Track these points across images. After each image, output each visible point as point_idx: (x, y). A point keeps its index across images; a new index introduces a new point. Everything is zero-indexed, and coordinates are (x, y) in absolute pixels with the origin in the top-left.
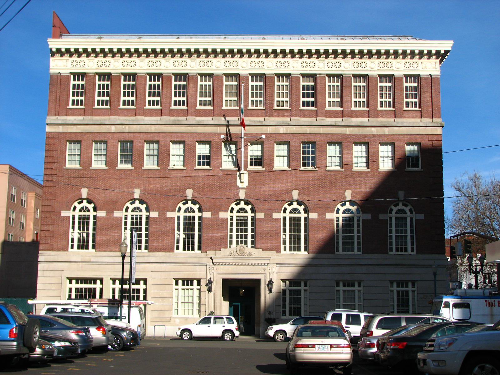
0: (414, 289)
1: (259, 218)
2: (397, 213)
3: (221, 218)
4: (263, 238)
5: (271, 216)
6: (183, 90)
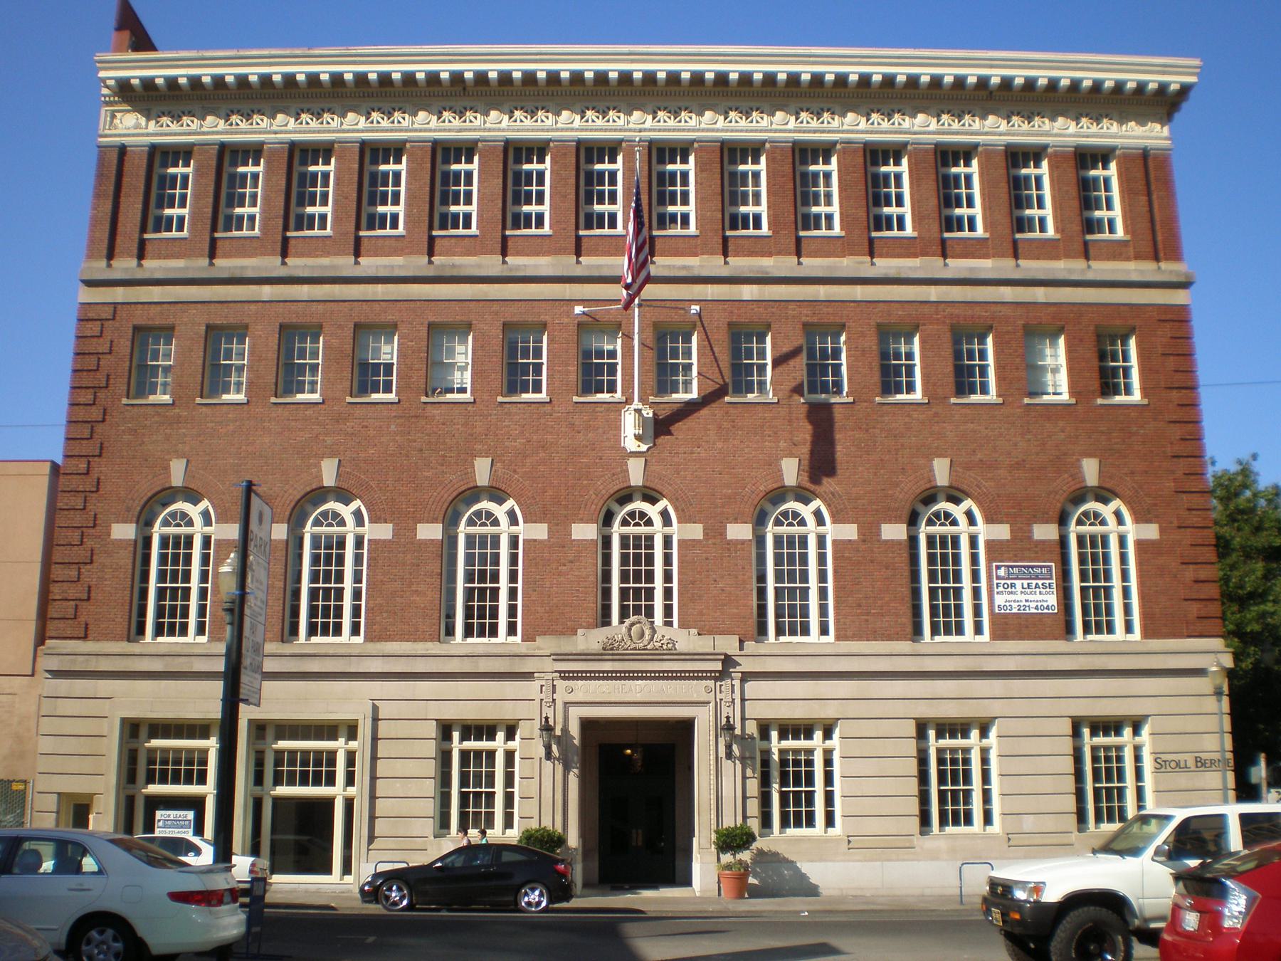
5: (723, 533)
6: (537, 186)
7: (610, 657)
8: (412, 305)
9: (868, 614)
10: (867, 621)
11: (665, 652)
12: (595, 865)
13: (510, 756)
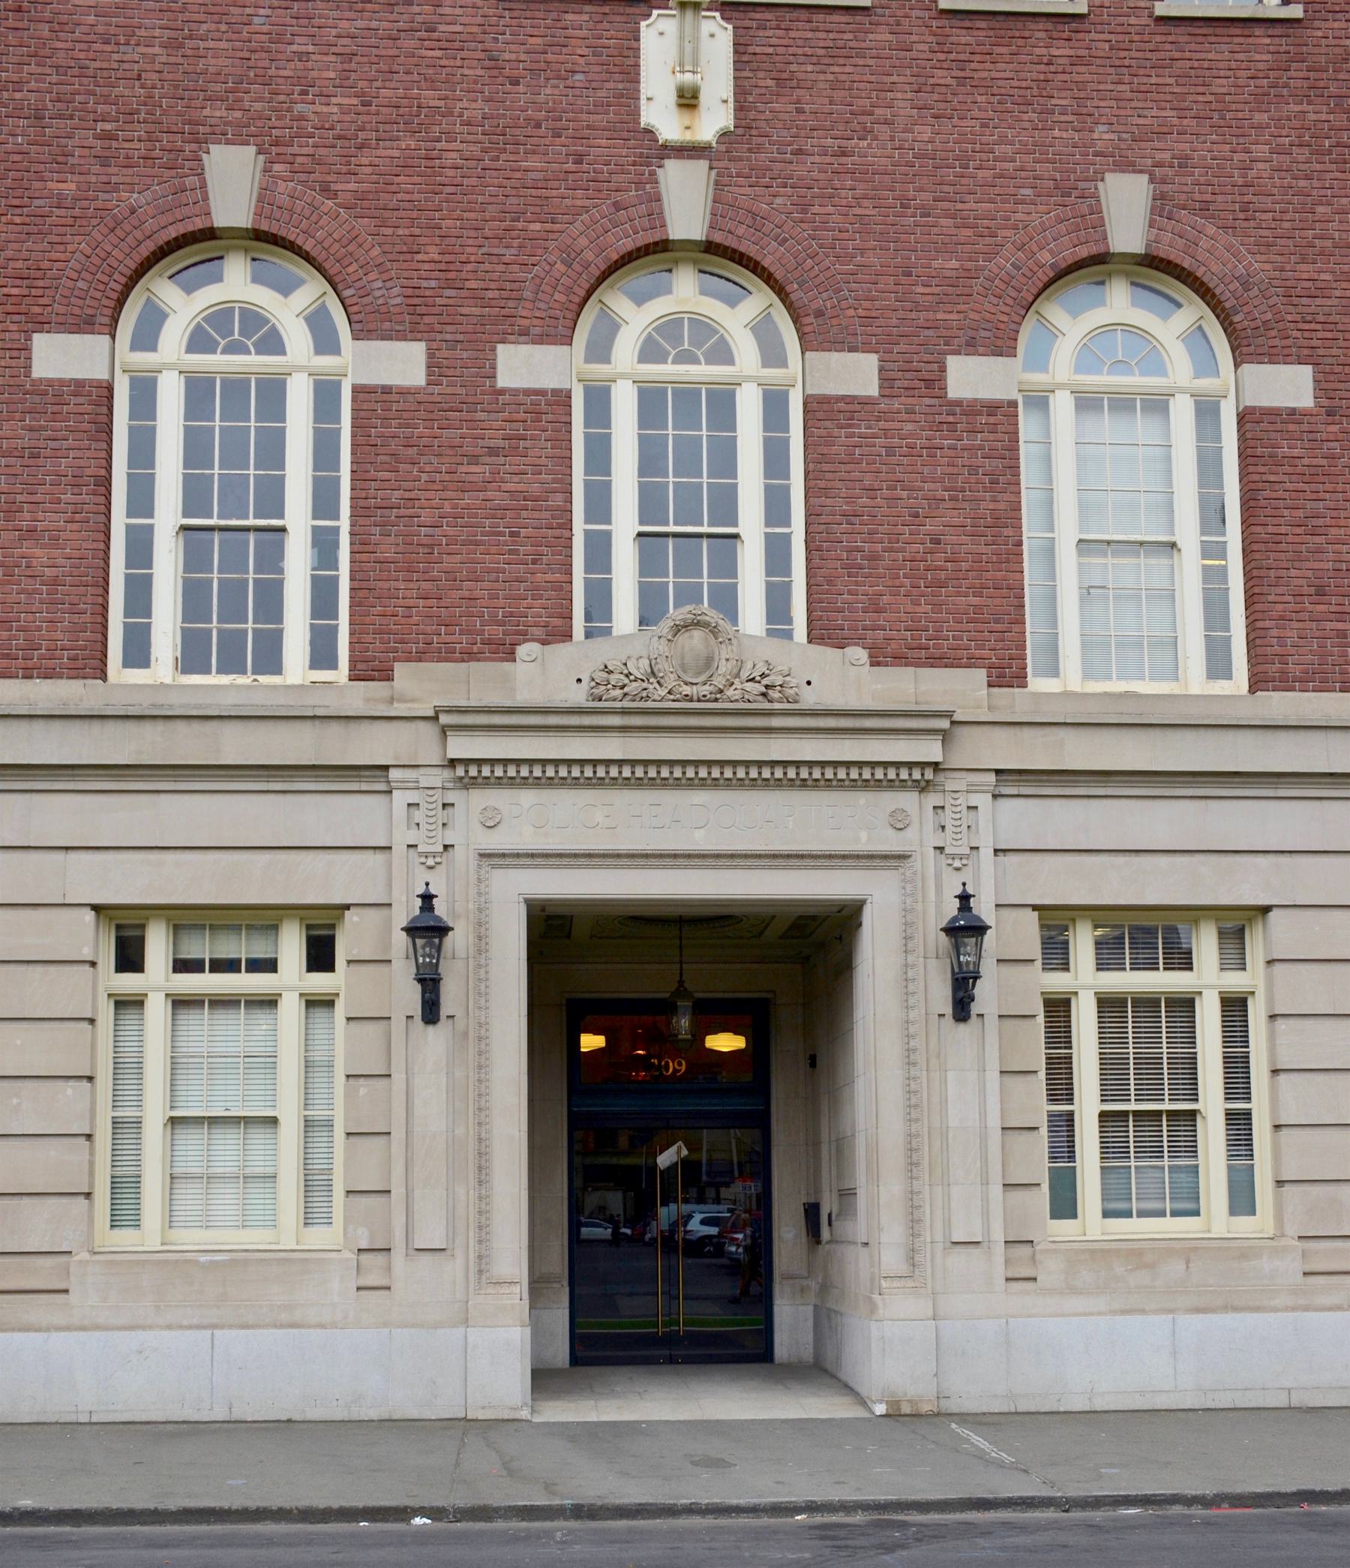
0: (1235, 981)
1: (843, 398)
2: (199, 342)
3: (515, 392)
4: (874, 557)
5: (935, 382)
7: (262, 1223)
11: (777, 706)
12: (559, 1318)
13: (1235, 1006)
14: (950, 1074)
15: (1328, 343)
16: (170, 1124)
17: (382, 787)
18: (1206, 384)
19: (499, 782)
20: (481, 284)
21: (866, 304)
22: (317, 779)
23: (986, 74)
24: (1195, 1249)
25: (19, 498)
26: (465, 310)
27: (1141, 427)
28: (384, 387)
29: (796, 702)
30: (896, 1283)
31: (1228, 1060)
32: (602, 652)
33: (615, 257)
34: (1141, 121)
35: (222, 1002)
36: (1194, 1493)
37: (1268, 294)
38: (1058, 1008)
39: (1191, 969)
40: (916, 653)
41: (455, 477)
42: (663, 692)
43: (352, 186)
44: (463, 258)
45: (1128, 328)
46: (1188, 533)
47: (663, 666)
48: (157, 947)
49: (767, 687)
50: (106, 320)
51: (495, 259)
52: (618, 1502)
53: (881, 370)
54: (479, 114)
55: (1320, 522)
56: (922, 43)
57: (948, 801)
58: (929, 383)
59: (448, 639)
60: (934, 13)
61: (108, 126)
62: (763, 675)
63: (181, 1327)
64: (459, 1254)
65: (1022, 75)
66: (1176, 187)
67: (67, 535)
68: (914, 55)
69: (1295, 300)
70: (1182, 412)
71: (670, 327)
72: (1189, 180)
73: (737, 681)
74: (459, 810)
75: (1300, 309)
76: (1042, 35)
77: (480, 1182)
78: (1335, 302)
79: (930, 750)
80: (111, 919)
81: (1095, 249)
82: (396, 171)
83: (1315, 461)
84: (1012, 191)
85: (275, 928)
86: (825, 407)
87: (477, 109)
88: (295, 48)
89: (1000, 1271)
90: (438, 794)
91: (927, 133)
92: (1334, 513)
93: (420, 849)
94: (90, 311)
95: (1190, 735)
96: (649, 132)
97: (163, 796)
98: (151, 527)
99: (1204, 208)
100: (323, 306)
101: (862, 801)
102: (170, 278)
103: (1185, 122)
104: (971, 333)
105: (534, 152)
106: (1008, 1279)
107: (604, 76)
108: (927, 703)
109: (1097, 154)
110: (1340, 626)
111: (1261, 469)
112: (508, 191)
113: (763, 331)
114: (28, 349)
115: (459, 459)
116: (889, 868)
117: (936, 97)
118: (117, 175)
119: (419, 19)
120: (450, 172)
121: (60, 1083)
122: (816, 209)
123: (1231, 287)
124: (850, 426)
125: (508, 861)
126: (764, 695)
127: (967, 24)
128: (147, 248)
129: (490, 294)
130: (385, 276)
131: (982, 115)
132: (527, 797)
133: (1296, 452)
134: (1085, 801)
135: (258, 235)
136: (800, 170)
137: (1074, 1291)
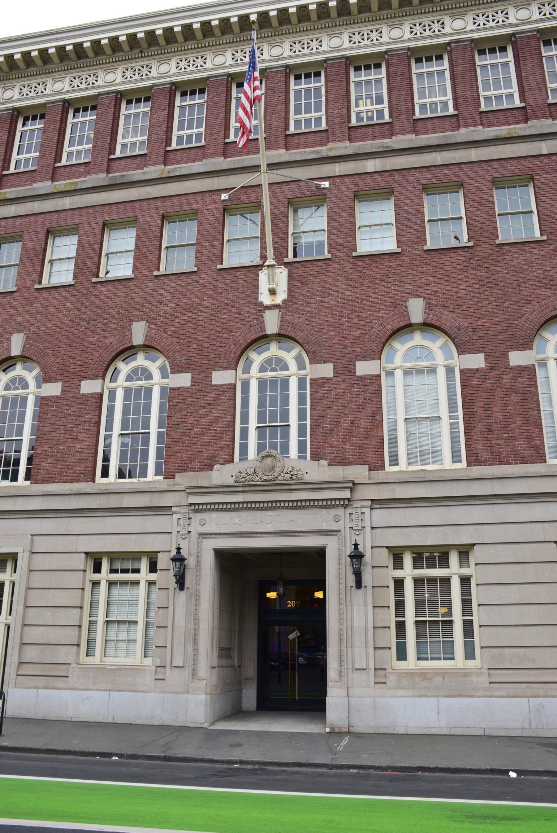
0: (465, 572)
1: (321, 379)
3: (217, 386)
4: (331, 430)
5: (352, 370)
8: (92, 210)
9: (498, 438)
10: (499, 445)
13: (465, 581)
14: (355, 607)
15: (489, 346)
16: (106, 624)
17: (171, 513)
18: (449, 362)
19: (205, 510)
20: (209, 354)
21: (329, 348)
22: (151, 511)
23: (368, 273)
24: (447, 673)
25: (74, 429)
26: (203, 362)
27: (426, 379)
28: (178, 387)
29: (301, 480)
30: (334, 683)
31: (463, 601)
32: (242, 466)
33: (249, 341)
34: (421, 282)
35: (124, 583)
36: (378, 765)
37: (467, 331)
38: (399, 583)
39: (449, 568)
40: (345, 461)
41: (198, 413)
42: (258, 479)
43: (172, 329)
44: (203, 346)
45: (421, 347)
46: (444, 413)
47: (258, 470)
48: (105, 565)
49: (292, 475)
50: (234, 366)
51: (213, 346)
52: (178, 756)
53: (485, 358)
54: (210, 304)
55: (489, 406)
56: (347, 267)
57: (354, 511)
58: (350, 371)
59: (194, 464)
60: (351, 257)
61: (107, 321)
62: (291, 472)
63: (100, 690)
64: (187, 668)
65: (380, 272)
66: (433, 301)
67: (86, 439)
68: (345, 270)
69: (477, 333)
70: (441, 372)
71: (269, 361)
72: (438, 298)
73: (282, 474)
74: (193, 521)
75: (479, 335)
76: (387, 259)
77: (195, 644)
78: (491, 332)
79: (347, 494)
80: (92, 556)
81: (406, 323)
82: (185, 323)
83: (486, 385)
84: (378, 307)
85: (139, 559)
86: (316, 382)
87: (209, 302)
88: (159, 292)
89: (372, 680)
90: (187, 515)
91: (348, 293)
92: (494, 403)
93: (181, 533)
94: (97, 373)
95: (441, 484)
96: (261, 303)
97: (107, 518)
98: (248, 427)
99: (444, 306)
100: (165, 365)
101: (324, 512)
102: (123, 361)
103: (436, 280)
104: (364, 354)
105: (226, 313)
106: (375, 683)
107: (248, 288)
108: (347, 478)
109: (406, 293)
110: (498, 442)
111: (467, 390)
112: (218, 325)
113: (443, 347)
114: (80, 385)
115: (199, 408)
116: (334, 535)
117: (352, 282)
118: (108, 334)
119: (194, 279)
120: (201, 322)
121: (72, 609)
122: (313, 320)
123: (454, 330)
124: (324, 387)
125: (208, 536)
126: (291, 478)
127: (362, 259)
128: (114, 353)
129: (211, 356)
130: (180, 354)
131: (368, 285)
132: (214, 515)
133: (479, 383)
134: (405, 509)
135: (145, 346)
136: (308, 309)
137: (399, 687)
